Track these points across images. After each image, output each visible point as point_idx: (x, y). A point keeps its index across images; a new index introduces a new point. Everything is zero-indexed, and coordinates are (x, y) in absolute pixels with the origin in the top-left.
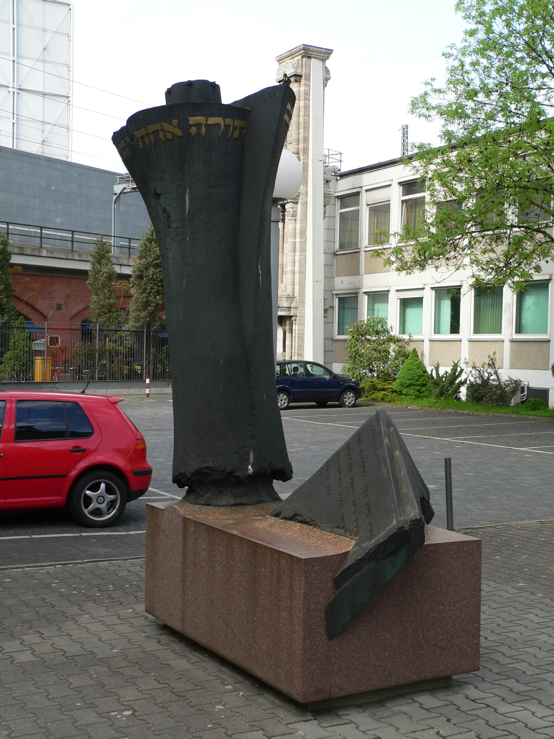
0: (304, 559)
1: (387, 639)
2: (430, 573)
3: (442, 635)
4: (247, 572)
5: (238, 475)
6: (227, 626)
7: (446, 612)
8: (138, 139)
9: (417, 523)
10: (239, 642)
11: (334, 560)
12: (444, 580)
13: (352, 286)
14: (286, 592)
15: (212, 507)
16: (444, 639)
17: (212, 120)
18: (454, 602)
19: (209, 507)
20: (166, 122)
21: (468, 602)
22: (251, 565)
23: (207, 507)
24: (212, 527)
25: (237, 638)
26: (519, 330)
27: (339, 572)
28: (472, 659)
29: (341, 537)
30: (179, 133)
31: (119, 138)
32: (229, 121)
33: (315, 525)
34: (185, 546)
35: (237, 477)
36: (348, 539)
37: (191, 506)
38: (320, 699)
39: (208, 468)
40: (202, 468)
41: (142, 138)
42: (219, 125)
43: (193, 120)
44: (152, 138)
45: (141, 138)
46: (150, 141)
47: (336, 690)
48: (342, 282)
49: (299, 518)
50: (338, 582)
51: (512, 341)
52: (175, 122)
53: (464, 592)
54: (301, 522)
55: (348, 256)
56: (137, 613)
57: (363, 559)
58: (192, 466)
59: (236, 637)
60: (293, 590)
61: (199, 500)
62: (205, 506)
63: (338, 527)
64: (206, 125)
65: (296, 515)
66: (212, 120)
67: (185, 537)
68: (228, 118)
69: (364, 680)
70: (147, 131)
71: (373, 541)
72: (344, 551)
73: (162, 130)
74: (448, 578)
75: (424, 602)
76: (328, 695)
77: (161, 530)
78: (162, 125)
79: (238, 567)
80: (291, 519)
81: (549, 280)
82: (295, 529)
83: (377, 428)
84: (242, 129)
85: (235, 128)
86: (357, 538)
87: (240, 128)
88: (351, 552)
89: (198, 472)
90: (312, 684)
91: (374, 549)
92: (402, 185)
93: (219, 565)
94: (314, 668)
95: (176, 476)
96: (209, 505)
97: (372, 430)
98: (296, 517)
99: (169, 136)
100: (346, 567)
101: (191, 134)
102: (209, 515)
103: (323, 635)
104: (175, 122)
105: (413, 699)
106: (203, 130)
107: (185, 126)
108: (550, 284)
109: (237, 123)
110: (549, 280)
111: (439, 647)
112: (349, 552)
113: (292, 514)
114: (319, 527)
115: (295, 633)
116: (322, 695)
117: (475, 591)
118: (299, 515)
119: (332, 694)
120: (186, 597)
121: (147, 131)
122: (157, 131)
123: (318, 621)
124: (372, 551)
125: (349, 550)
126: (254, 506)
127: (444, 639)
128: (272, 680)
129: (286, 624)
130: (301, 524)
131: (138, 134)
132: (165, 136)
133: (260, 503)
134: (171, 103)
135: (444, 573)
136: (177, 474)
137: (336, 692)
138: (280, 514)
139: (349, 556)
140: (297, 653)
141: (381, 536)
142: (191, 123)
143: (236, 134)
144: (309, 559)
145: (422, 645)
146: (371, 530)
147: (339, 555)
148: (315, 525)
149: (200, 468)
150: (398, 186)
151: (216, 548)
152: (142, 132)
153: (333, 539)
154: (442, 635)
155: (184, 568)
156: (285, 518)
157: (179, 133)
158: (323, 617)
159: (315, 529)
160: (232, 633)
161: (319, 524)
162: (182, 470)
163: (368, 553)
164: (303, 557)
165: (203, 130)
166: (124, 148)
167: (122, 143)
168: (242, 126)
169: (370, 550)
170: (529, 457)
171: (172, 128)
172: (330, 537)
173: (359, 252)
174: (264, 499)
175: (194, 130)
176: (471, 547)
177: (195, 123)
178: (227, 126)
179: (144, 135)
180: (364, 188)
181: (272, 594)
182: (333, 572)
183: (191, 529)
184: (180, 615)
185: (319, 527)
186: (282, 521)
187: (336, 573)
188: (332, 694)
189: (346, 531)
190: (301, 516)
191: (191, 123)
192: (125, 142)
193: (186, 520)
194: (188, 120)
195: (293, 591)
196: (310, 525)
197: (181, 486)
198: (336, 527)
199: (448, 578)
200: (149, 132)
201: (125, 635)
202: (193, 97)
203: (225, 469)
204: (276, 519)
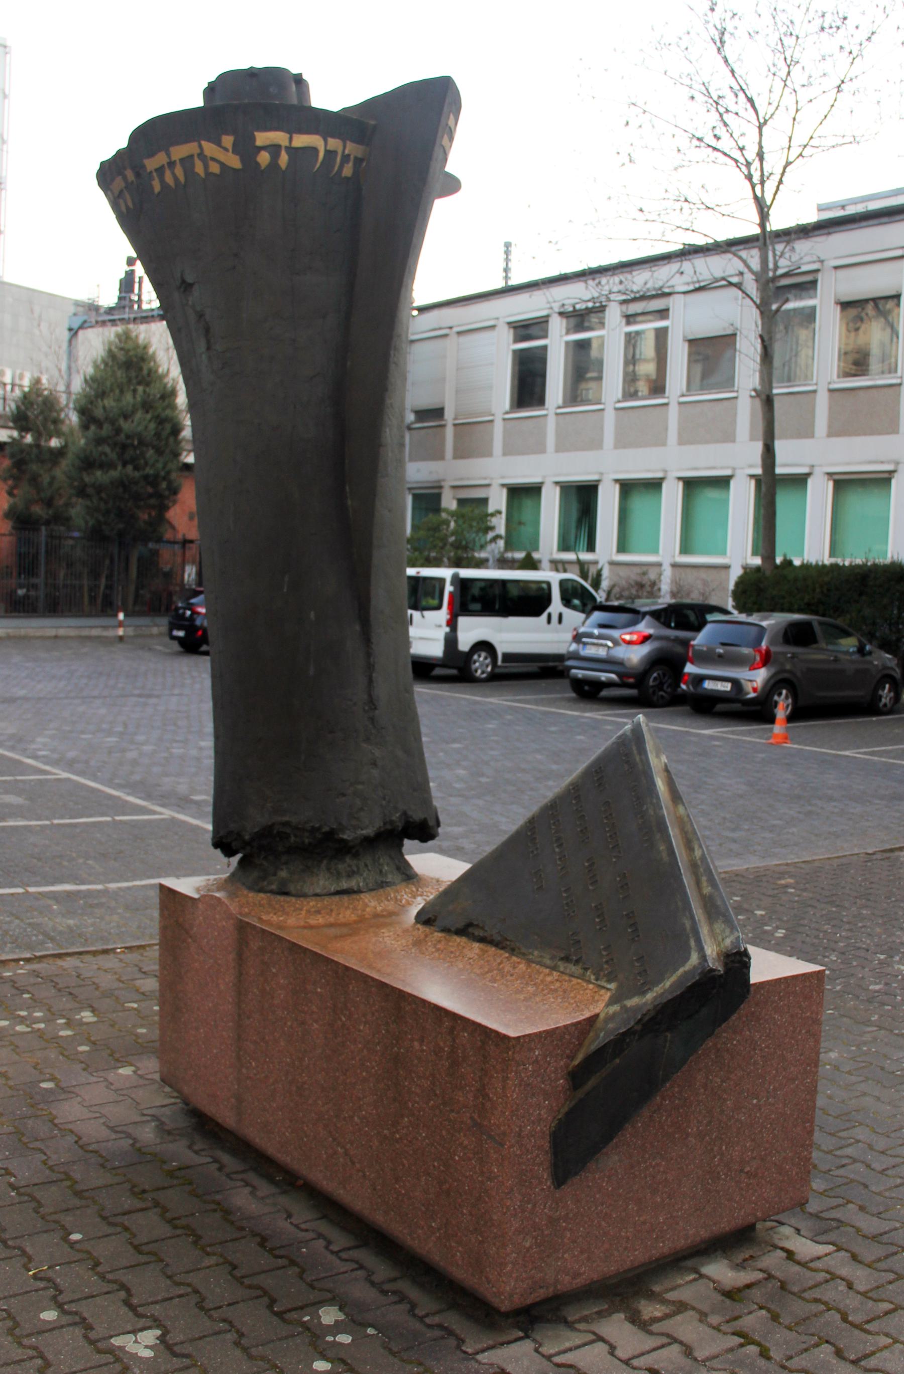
0: (514, 1038)
1: (659, 1172)
2: (738, 1041)
3: (752, 1151)
4: (378, 1044)
5: (345, 837)
6: (334, 1139)
7: (760, 1109)
8: (151, 172)
9: (738, 958)
10: (361, 1174)
11: (570, 1034)
12: (761, 1050)
13: (434, 477)
14: (470, 1096)
15: (293, 899)
16: (755, 1158)
17: (301, 141)
18: (775, 1089)
19: (288, 899)
20: (209, 140)
21: (797, 1086)
22: (387, 1031)
23: (281, 898)
24: (301, 947)
25: (358, 1166)
26: (685, 549)
27: (580, 1057)
28: (798, 1186)
29: (575, 981)
30: (235, 162)
31: (109, 174)
32: (334, 143)
33: (513, 951)
34: (240, 975)
35: (343, 840)
36: (591, 986)
37: (251, 895)
38: (538, 1299)
39: (286, 824)
40: (273, 824)
41: (160, 170)
42: (315, 150)
43: (262, 138)
44: (179, 171)
45: (156, 170)
46: (176, 179)
47: (567, 1278)
48: (418, 471)
49: (478, 933)
50: (577, 1077)
51: (675, 566)
52: (228, 140)
53: (792, 1069)
54: (482, 940)
55: (430, 431)
56: (141, 1077)
57: (629, 1033)
58: (256, 819)
59: (353, 1163)
60: (487, 1095)
61: (265, 883)
62: (279, 897)
63: (566, 959)
64: (289, 149)
65: (470, 925)
66: (301, 141)
67: (240, 958)
68: (333, 137)
69: (616, 1253)
70: (169, 157)
71: (650, 996)
72: (587, 1014)
73: (201, 155)
74: (767, 1047)
75: (725, 1096)
76: (551, 1289)
77: (191, 937)
78: (200, 146)
79: (360, 1031)
80: (460, 932)
81: (808, 475)
82: (470, 955)
83: (638, 758)
84: (358, 161)
85: (346, 158)
86: (612, 986)
87: (356, 158)
88: (602, 1016)
89: (267, 832)
90: (524, 1275)
91: (652, 1013)
92: (515, 328)
93: (316, 1021)
94: (528, 1244)
95: (221, 837)
96: (286, 894)
97: (627, 762)
98: (470, 930)
99: (215, 168)
100: (594, 1047)
101: (258, 164)
102: (287, 914)
103: (546, 1180)
104: (228, 140)
105: (697, 1271)
106: (284, 159)
107: (246, 149)
108: (893, 482)
109: (352, 148)
110: (808, 475)
111: (747, 1173)
112: (597, 1016)
113: (460, 924)
114: (524, 954)
115: (489, 1179)
116: (542, 1291)
117: (809, 1065)
118: (477, 926)
119: (559, 1287)
120: (244, 1071)
121: (169, 157)
122: (191, 157)
123: (538, 1156)
124: (647, 1018)
125: (597, 1011)
126: (373, 893)
127: (755, 1158)
128: (437, 1258)
129: (470, 1159)
130: (482, 945)
131: (151, 164)
132: (206, 167)
133: (382, 887)
134: (218, 102)
135: (760, 1037)
136: (222, 833)
137: (566, 1283)
138: (435, 920)
139: (599, 1024)
140: (495, 1217)
141: (666, 986)
142: (259, 143)
143: (348, 171)
144: (524, 1036)
145: (719, 1173)
146: (643, 973)
147: (579, 1023)
148: (513, 950)
149: (270, 823)
150: (506, 327)
151: (309, 987)
152: (160, 159)
153: (558, 984)
154: (752, 1151)
155: (239, 1015)
156: (446, 930)
157: (235, 162)
158: (547, 1146)
159: (514, 959)
160: (346, 1153)
161: (523, 950)
162: (233, 826)
163: (640, 1020)
164: (512, 1033)
165: (284, 159)
166: (121, 191)
167: (119, 183)
168: (359, 156)
169: (644, 1015)
170: (719, 746)
171: (222, 154)
172: (549, 979)
173: (444, 426)
174: (389, 878)
175: (264, 158)
176: (808, 984)
177: (268, 143)
178: (330, 154)
179: (163, 166)
180: (456, 329)
181: (436, 1095)
182: (568, 1057)
183: (255, 945)
184: (233, 1100)
185: (524, 954)
186: (440, 934)
187: (572, 1060)
188: (559, 1287)
189: (586, 969)
190: (483, 928)
191: (259, 143)
192: (125, 178)
193: (243, 928)
194: (253, 139)
195: (486, 1096)
196: (503, 948)
197: (229, 852)
198: (562, 959)
199: (767, 1047)
200: (173, 159)
201: (124, 1128)
202: (254, 99)
203: (319, 829)
204: (427, 929)
